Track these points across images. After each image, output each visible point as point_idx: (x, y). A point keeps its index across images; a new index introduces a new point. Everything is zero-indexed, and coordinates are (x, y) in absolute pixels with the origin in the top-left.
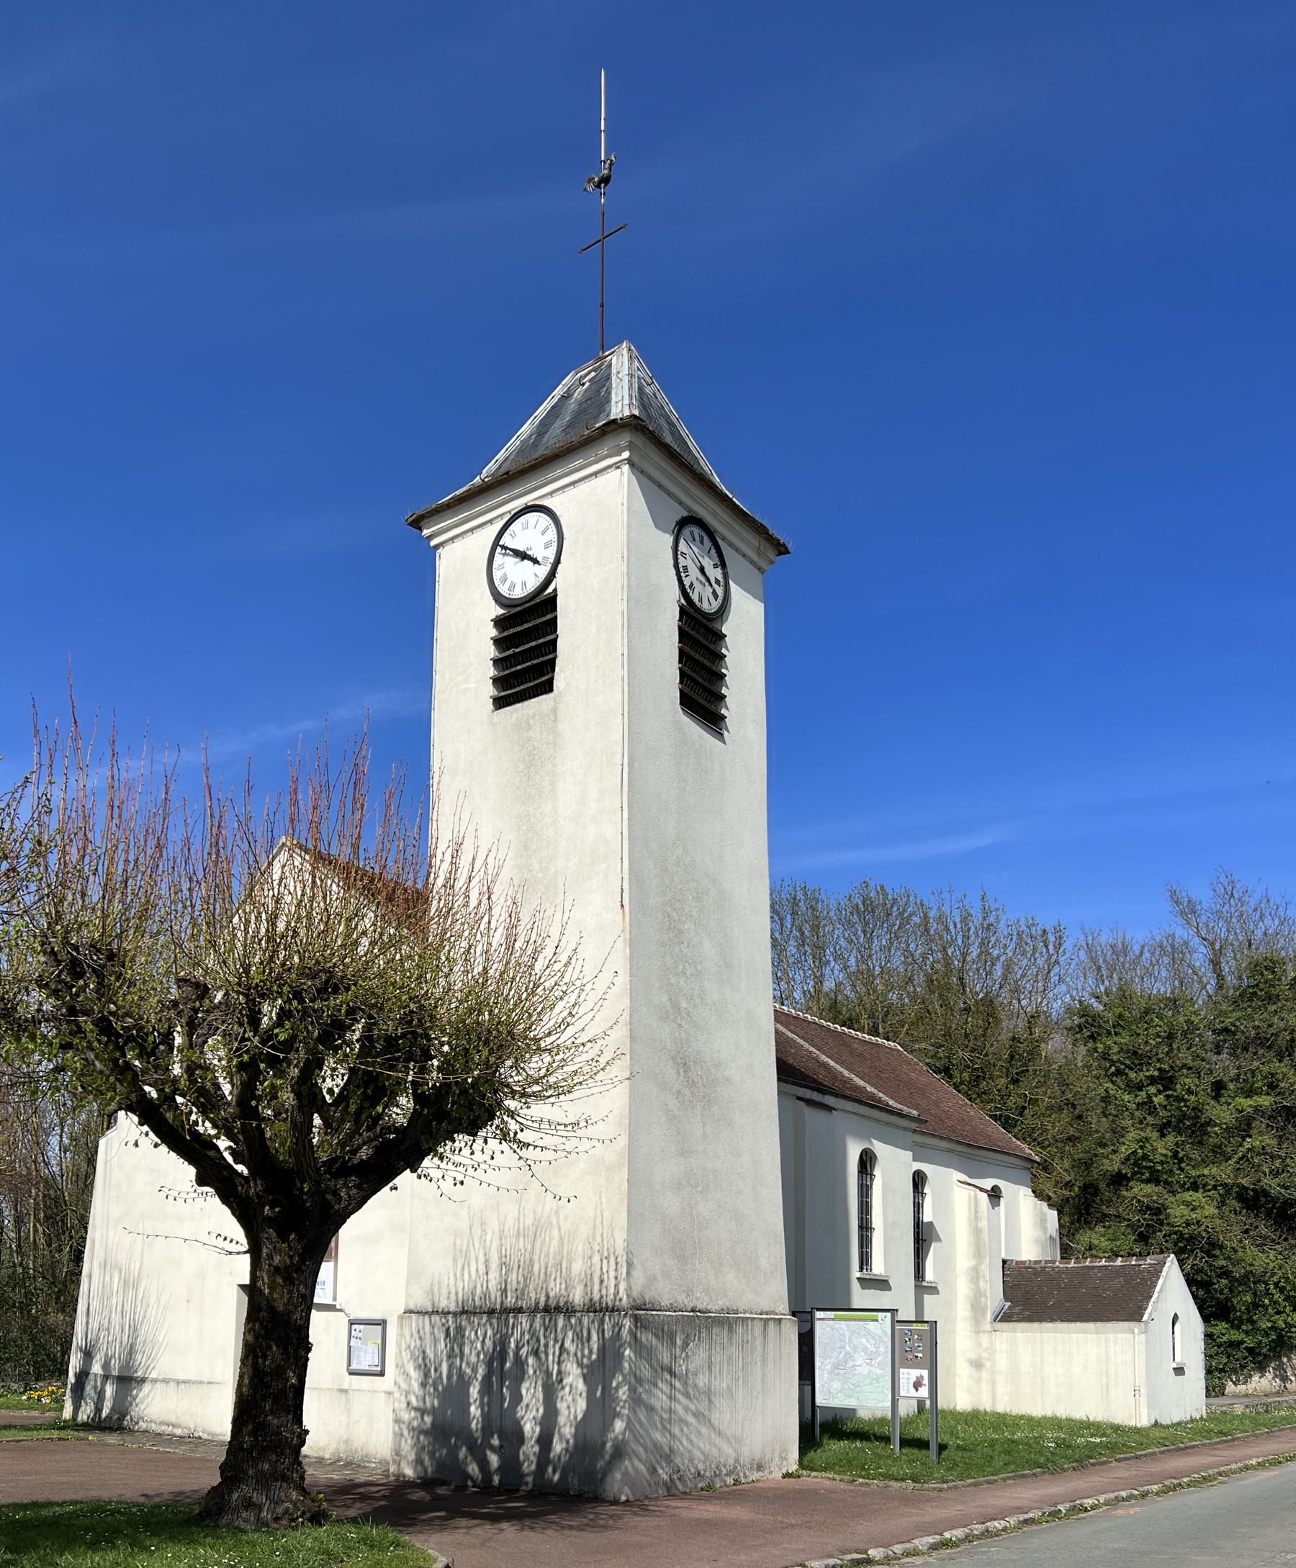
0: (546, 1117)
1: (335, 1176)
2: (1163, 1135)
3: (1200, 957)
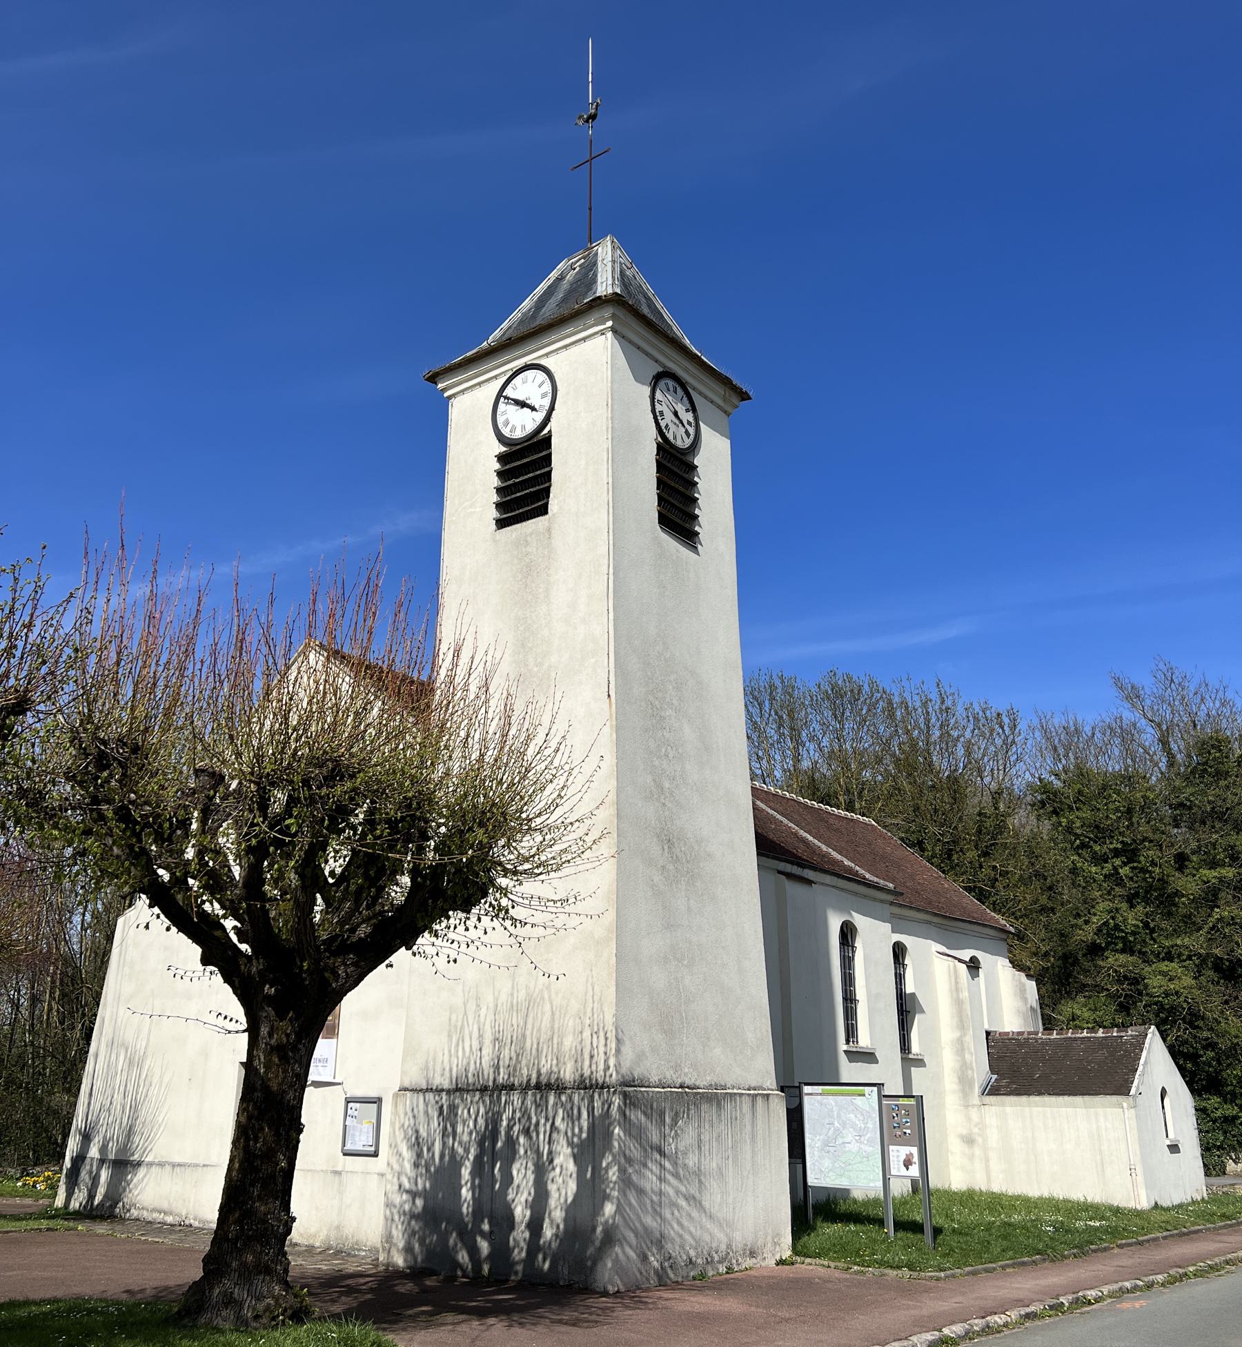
0: (536, 894)
1: (335, 954)
2: (1132, 906)
3: (1149, 736)
